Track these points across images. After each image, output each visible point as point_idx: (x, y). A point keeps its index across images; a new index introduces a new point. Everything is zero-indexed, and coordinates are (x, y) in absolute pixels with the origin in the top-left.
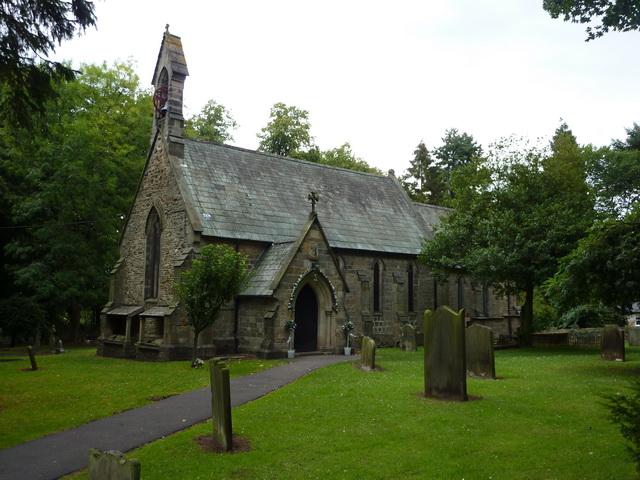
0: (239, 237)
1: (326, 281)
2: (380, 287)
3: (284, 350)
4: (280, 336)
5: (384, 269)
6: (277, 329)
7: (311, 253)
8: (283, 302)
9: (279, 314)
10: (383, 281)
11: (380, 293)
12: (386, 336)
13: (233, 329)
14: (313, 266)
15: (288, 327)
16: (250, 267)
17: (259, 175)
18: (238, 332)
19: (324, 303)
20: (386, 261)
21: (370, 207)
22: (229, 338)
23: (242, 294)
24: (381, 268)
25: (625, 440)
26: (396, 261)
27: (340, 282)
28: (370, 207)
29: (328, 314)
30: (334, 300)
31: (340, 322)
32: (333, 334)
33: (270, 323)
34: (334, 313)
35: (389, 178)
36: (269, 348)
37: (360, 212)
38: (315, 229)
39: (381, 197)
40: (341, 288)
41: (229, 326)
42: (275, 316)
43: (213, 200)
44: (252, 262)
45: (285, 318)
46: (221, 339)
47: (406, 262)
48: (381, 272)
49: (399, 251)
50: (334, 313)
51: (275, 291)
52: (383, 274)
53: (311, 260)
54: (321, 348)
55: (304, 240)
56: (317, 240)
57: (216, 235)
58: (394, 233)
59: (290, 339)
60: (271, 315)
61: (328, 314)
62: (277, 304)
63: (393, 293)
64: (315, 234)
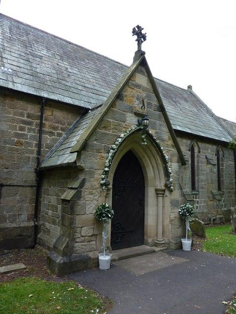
0: (45, 95)
1: (158, 147)
2: (196, 166)
3: (91, 255)
4: (86, 231)
5: (199, 152)
6: (79, 220)
7: (137, 105)
8: (91, 174)
9: (85, 192)
10: (198, 163)
11: (196, 175)
12: (203, 213)
13: (31, 211)
14: (139, 124)
15: (100, 215)
16: (59, 135)
17: (84, 61)
18: (40, 216)
19: (154, 179)
20: (200, 144)
21: (180, 103)
22: (26, 224)
23: (43, 166)
24: (196, 150)
25: (83, 165)
26: (208, 145)
27: (174, 150)
28: (180, 103)
29: (159, 193)
30: (167, 174)
31: (174, 204)
32: (167, 222)
33: (70, 206)
34: (167, 193)
35: (188, 91)
36: (64, 254)
37: (173, 105)
38: (141, 72)
39: (186, 100)
40: (176, 158)
41: (28, 209)
42: (78, 196)
43: (26, 62)
44: (62, 129)
45: (95, 198)
46: (14, 225)
47: (215, 147)
48: (196, 154)
49: (209, 137)
50: (167, 193)
51: (79, 156)
52: (198, 156)
53: (137, 114)
54: (150, 240)
55: (126, 84)
56: (144, 89)
57: (10, 86)
58: (202, 124)
59: (106, 235)
60: (69, 195)
61: (159, 193)
62: (82, 177)
63: (206, 173)
64: (141, 80)
